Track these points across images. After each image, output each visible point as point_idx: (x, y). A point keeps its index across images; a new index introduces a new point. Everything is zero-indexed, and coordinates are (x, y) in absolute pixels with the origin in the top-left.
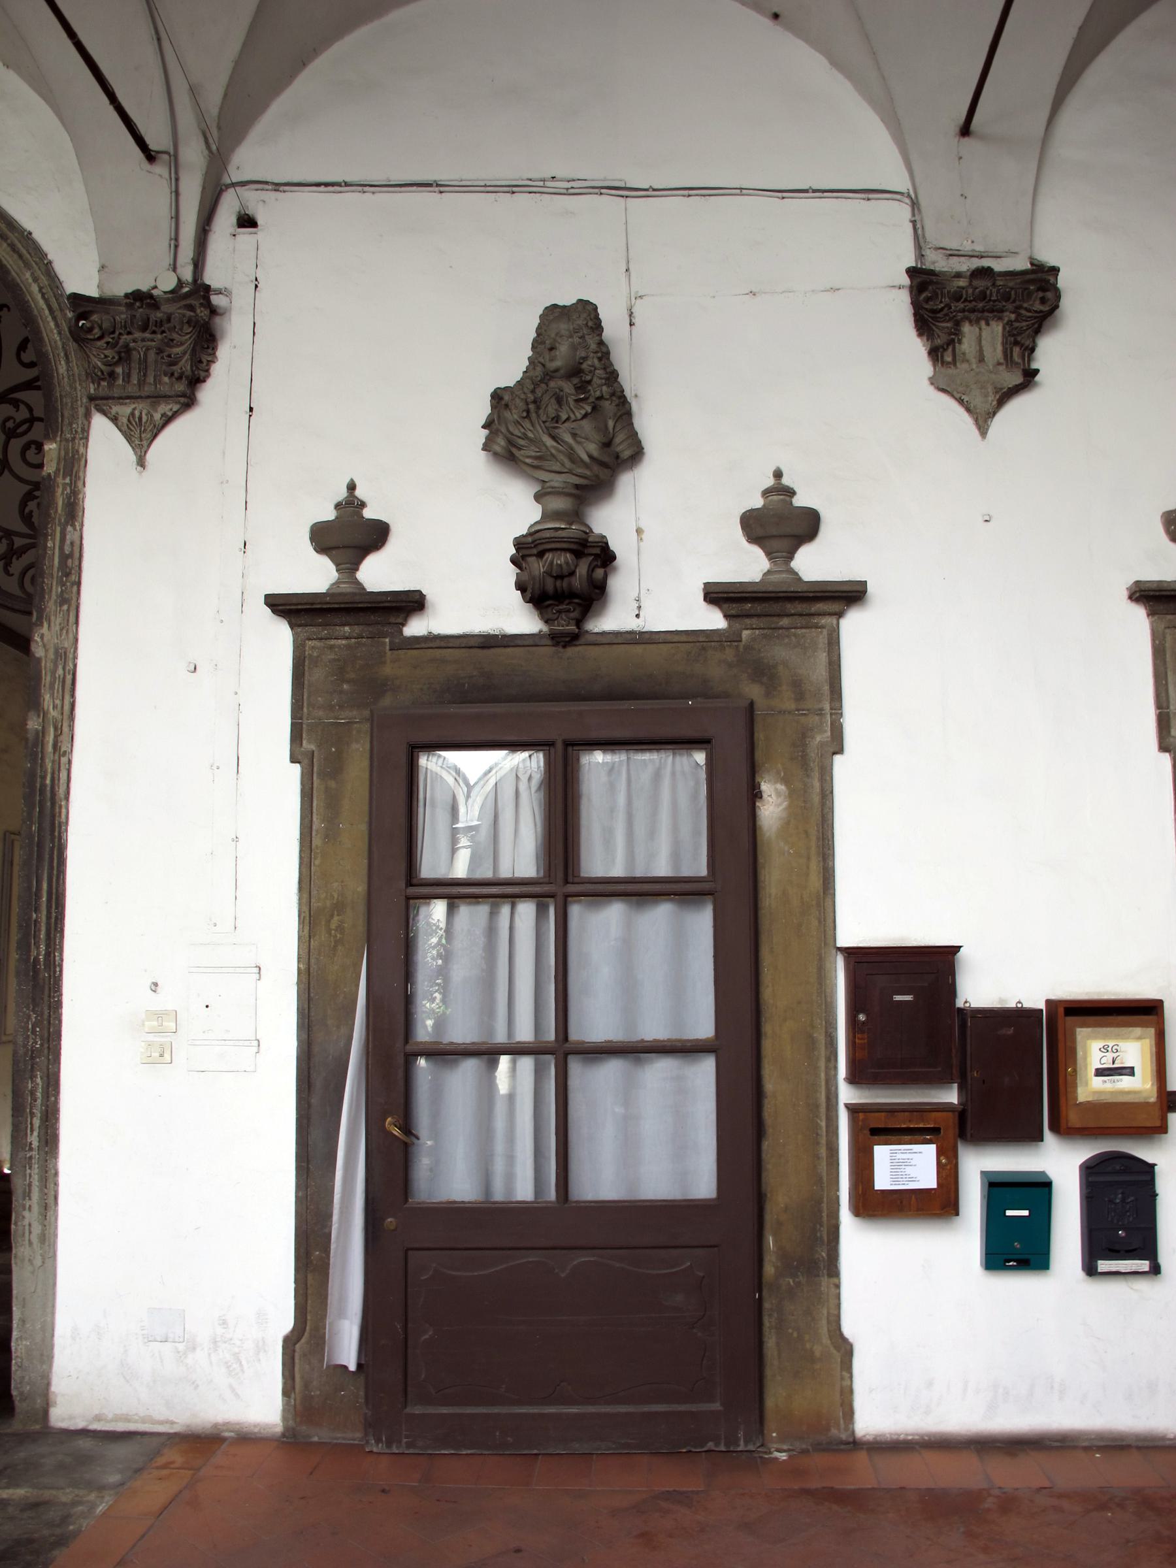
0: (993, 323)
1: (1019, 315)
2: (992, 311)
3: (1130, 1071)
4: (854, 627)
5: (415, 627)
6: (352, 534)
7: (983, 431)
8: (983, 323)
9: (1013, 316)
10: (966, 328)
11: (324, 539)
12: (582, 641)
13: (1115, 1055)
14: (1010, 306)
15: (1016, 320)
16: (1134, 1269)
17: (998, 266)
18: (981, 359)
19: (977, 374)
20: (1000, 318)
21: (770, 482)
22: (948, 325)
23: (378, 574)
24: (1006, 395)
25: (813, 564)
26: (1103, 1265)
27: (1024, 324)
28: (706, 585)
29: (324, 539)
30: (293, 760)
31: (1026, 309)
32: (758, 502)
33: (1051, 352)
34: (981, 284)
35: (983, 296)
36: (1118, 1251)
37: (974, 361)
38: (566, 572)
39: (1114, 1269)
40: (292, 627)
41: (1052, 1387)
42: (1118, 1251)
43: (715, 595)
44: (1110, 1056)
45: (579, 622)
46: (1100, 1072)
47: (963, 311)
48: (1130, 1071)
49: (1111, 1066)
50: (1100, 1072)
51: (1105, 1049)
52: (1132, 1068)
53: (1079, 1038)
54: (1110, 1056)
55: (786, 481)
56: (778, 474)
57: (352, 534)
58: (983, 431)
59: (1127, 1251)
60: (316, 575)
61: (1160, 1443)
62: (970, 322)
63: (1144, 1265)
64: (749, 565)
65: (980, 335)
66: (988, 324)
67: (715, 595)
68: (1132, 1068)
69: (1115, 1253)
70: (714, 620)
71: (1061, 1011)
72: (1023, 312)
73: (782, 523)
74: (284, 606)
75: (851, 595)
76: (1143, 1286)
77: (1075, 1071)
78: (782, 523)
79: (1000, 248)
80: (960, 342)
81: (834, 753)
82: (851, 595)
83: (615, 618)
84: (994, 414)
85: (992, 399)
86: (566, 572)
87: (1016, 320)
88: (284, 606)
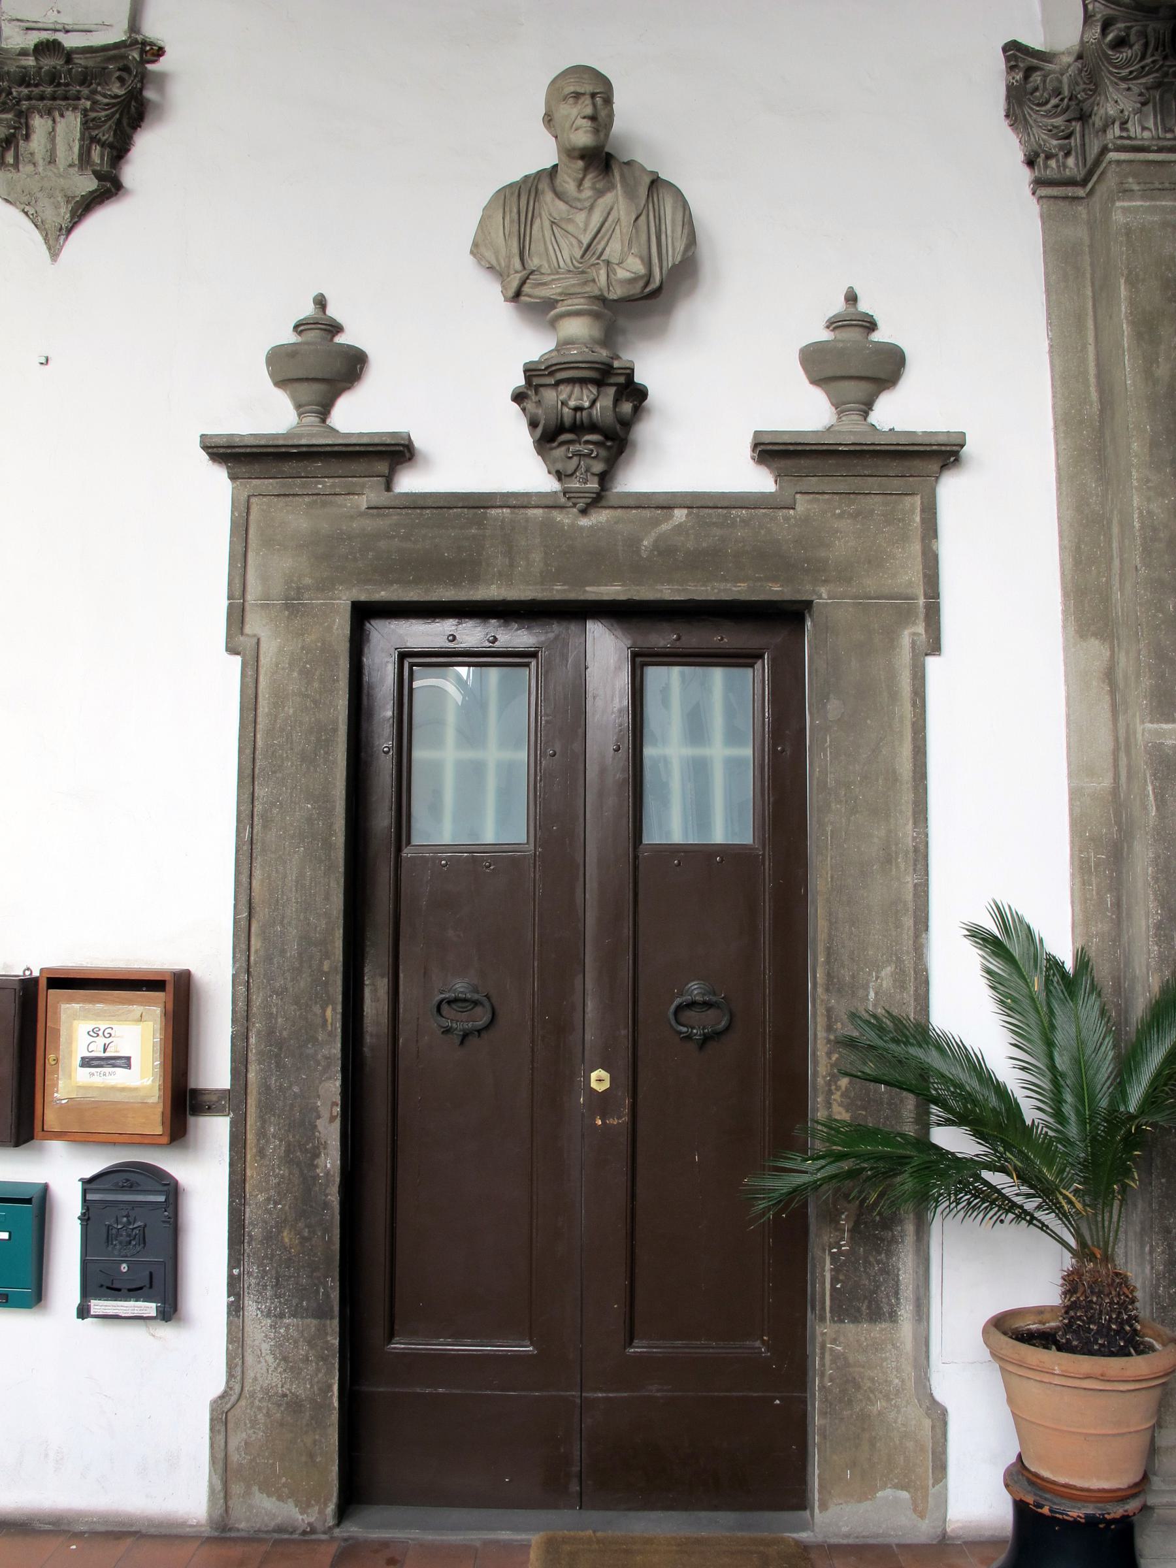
0: (69, 114)
1: (95, 102)
2: (66, 98)
3: (126, 1062)
4: (952, 491)
5: (409, 482)
6: (323, 363)
7: (54, 253)
8: (57, 114)
9: (88, 104)
10: (39, 124)
11: (285, 368)
12: (603, 503)
13: (107, 1041)
14: (85, 91)
15: (92, 109)
16: (137, 1313)
17: (71, 41)
18: (52, 161)
19: (42, 178)
20: (75, 108)
21: (308, 309)
22: (9, 116)
23: (356, 416)
24: (85, 206)
25: (897, 414)
26: (98, 1306)
27: (104, 113)
28: (202, 436)
29: (821, 365)
30: (232, 649)
31: (105, 96)
32: (825, 336)
33: (149, 154)
34: (48, 63)
35: (53, 78)
36: (119, 1290)
37: (41, 162)
38: (589, 413)
39: (111, 1312)
40: (233, 477)
41: (46, 1455)
42: (119, 1290)
43: (771, 451)
44: (101, 1041)
45: (605, 478)
46: (87, 1062)
47: (29, 98)
48: (126, 1062)
49: (102, 1055)
50: (87, 1062)
51: (94, 1033)
52: (128, 1059)
53: (63, 1017)
54: (101, 1041)
55: (864, 306)
56: (852, 298)
57: (323, 363)
58: (54, 253)
59: (130, 1290)
60: (274, 416)
61: (174, 1531)
62: (39, 112)
63: (149, 1308)
64: (809, 413)
65: (54, 129)
66: (62, 116)
67: (771, 451)
68: (128, 1059)
69: (114, 1291)
70: (762, 481)
71: (43, 984)
72: (99, 98)
73: (858, 361)
74: (232, 455)
75: (945, 454)
76: (165, 1331)
77: (57, 1060)
78: (858, 361)
79: (89, 21)
80: (27, 137)
81: (927, 655)
82: (945, 454)
83: (643, 477)
84: (69, 231)
85: (65, 212)
86: (589, 413)
87: (92, 109)
88: (232, 455)
